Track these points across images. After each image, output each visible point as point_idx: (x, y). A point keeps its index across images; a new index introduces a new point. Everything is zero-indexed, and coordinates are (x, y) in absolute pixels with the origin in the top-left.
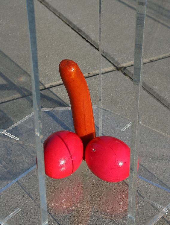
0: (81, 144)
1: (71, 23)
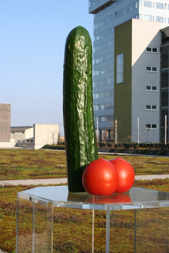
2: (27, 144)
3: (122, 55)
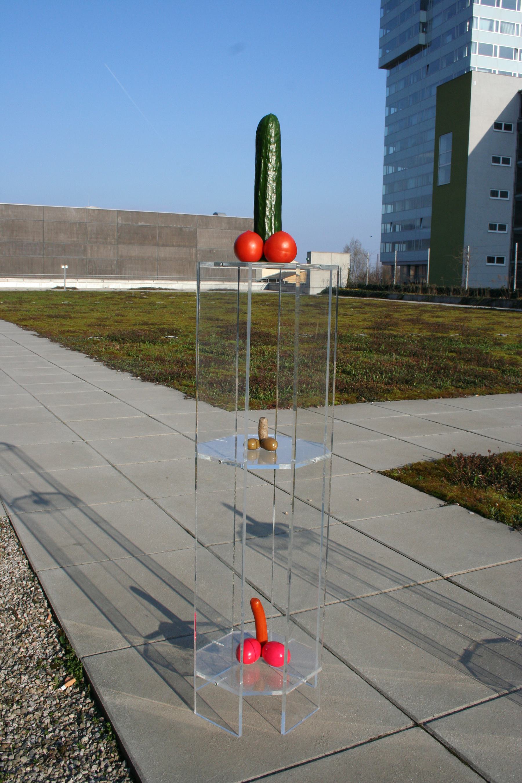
0: (260, 646)
1: (252, 583)
2: (287, 287)
3: (450, 135)
